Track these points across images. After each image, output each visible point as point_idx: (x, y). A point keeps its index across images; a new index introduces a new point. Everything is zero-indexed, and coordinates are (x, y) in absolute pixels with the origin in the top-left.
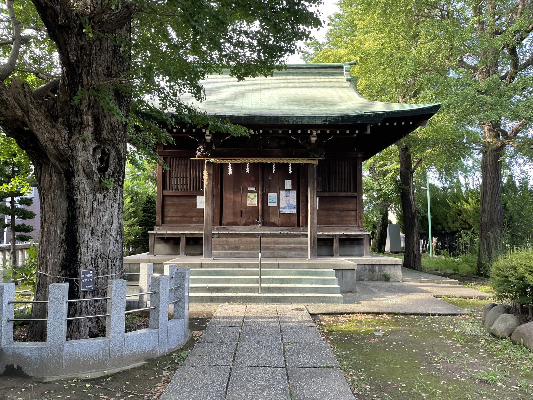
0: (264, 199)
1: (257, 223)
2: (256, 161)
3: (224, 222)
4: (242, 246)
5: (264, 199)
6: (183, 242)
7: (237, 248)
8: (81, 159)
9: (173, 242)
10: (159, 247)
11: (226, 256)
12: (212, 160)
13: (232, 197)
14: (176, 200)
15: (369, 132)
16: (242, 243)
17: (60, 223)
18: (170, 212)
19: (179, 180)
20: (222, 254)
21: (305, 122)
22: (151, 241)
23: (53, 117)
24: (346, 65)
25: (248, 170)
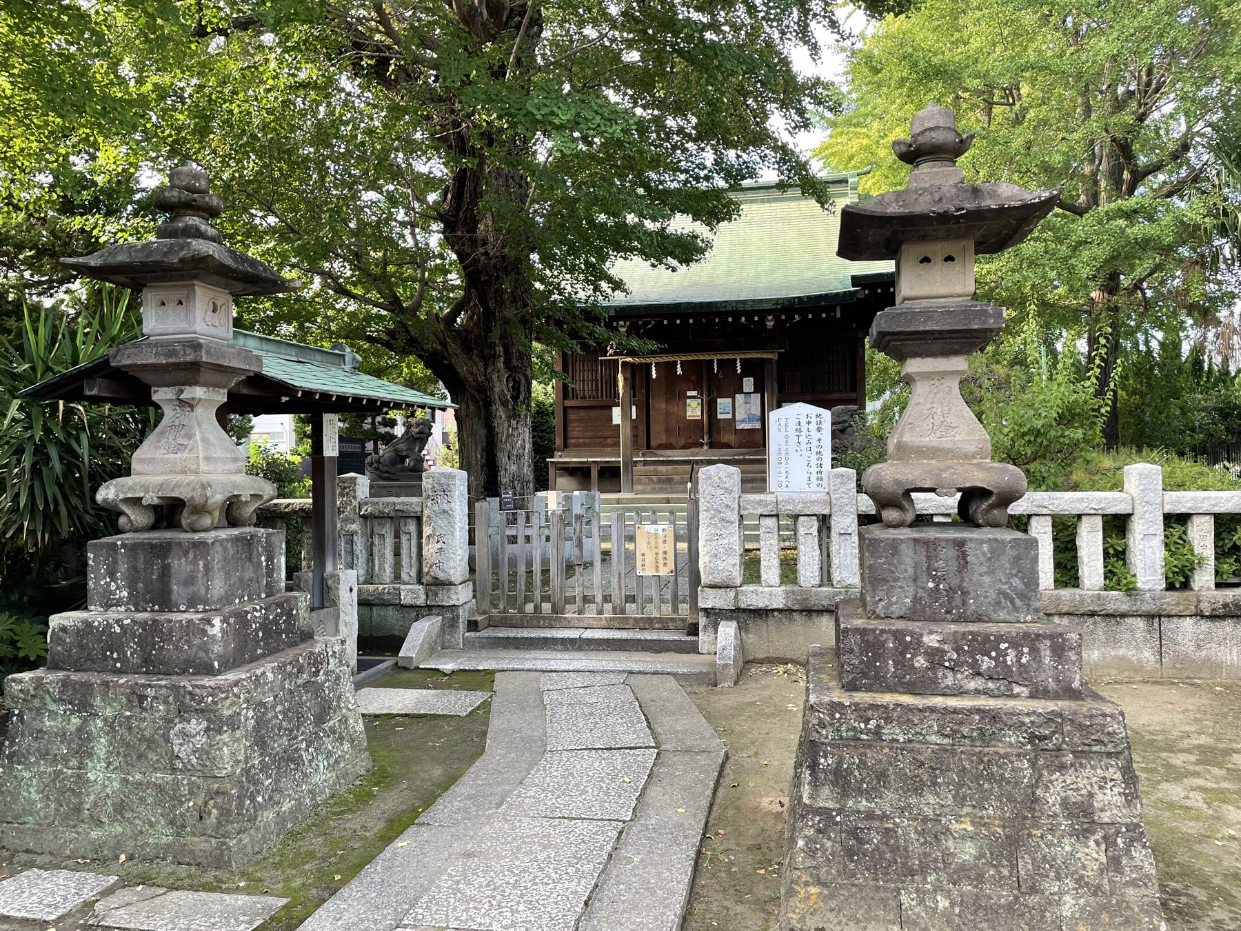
0: (711, 408)
1: (701, 445)
2: (690, 358)
3: (653, 443)
4: (677, 478)
5: (711, 408)
6: (594, 474)
7: (670, 481)
8: (496, 390)
9: (581, 474)
10: (562, 481)
11: (654, 491)
12: (629, 359)
13: (663, 406)
14: (582, 413)
15: (838, 315)
16: (678, 473)
17: (479, 448)
18: (576, 431)
19: (584, 383)
20: (648, 488)
21: (748, 307)
22: (552, 472)
23: (468, 349)
24: (852, 176)
25: (679, 371)
